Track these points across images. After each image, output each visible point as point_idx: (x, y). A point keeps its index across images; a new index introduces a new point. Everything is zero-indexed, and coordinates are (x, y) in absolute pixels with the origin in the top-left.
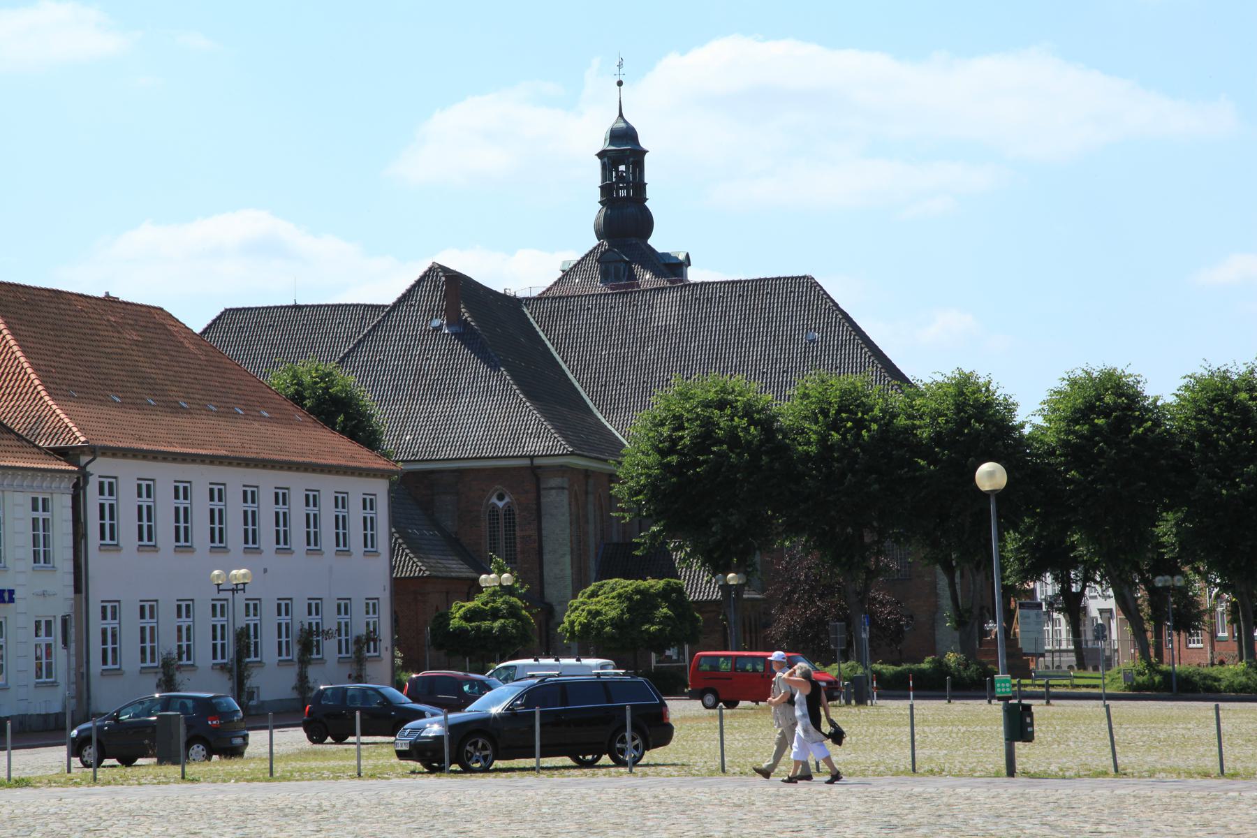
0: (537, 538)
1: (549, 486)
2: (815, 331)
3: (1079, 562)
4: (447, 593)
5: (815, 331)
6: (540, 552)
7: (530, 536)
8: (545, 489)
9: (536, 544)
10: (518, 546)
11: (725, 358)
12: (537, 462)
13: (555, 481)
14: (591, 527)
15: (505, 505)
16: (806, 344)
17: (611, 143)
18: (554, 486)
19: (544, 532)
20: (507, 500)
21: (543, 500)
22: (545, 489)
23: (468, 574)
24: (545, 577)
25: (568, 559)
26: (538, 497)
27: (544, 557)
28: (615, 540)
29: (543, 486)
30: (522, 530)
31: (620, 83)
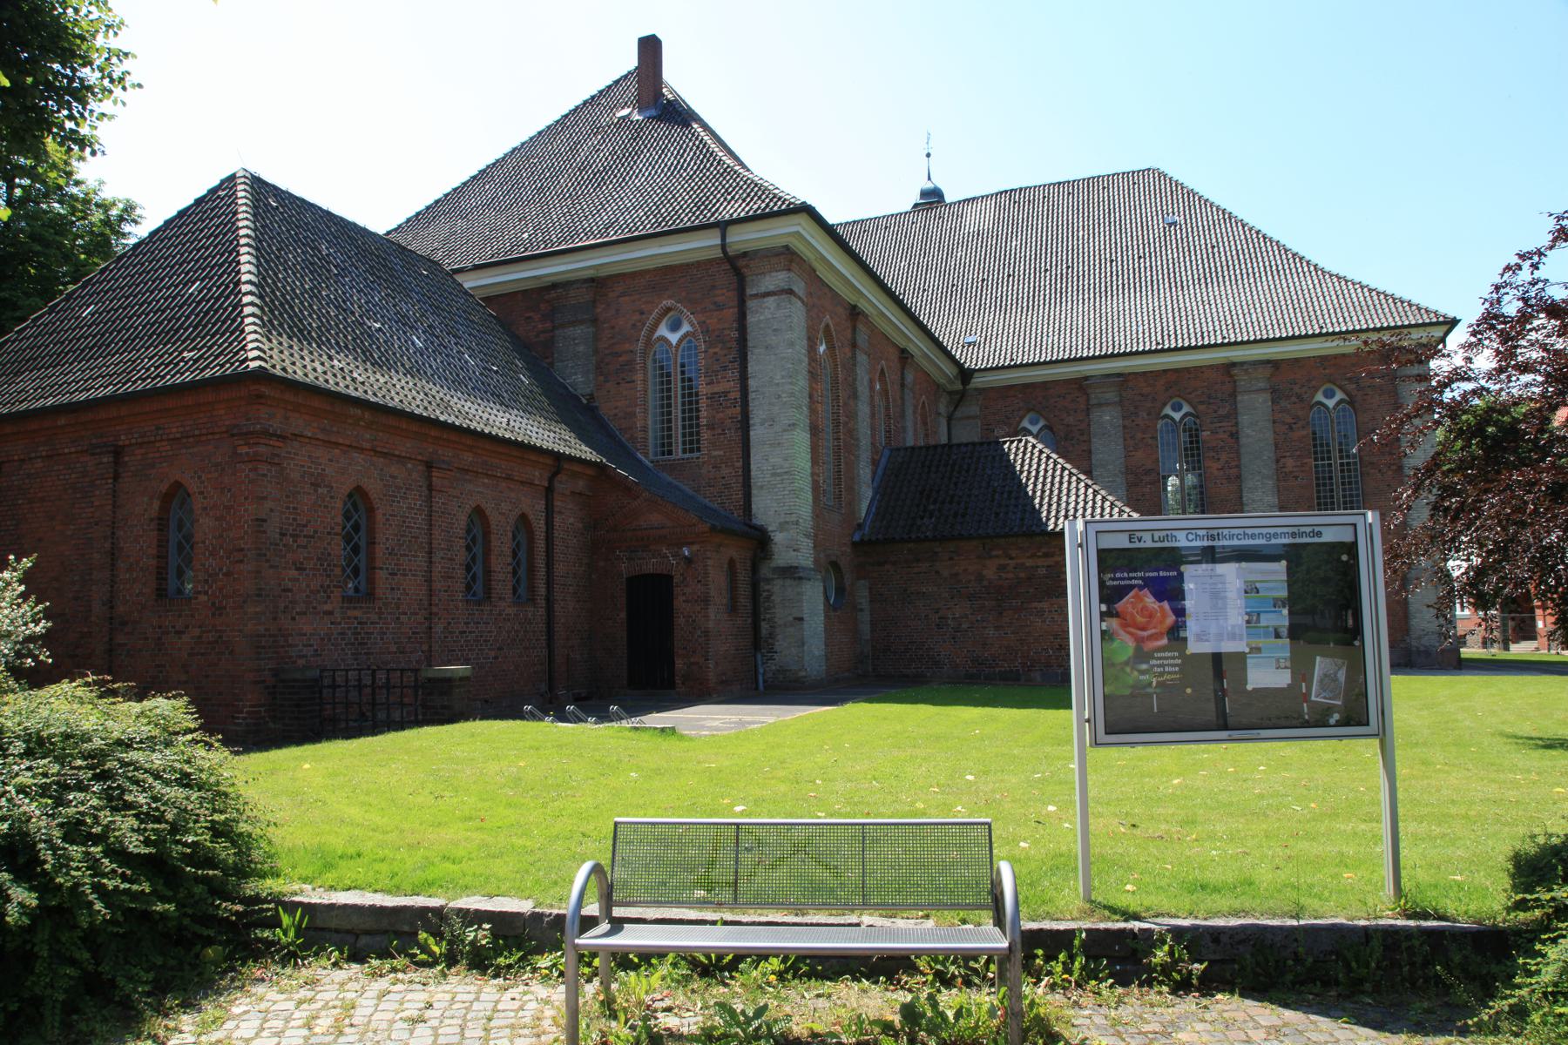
0: (738, 395)
1: (763, 290)
2: (1174, 214)
3: (170, 823)
4: (429, 466)
5: (1174, 214)
6: (745, 425)
7: (726, 393)
8: (756, 296)
9: (738, 409)
10: (703, 414)
11: (1057, 253)
12: (741, 238)
13: (775, 279)
14: (864, 409)
15: (680, 341)
16: (1165, 228)
17: (921, 198)
18: (772, 288)
19: (752, 383)
20: (686, 328)
21: (751, 319)
22: (756, 296)
23: (1392, 922)
24: (753, 473)
25: (802, 439)
26: (742, 316)
27: (752, 433)
28: (910, 442)
29: (749, 291)
30: (711, 383)
31: (928, 155)
